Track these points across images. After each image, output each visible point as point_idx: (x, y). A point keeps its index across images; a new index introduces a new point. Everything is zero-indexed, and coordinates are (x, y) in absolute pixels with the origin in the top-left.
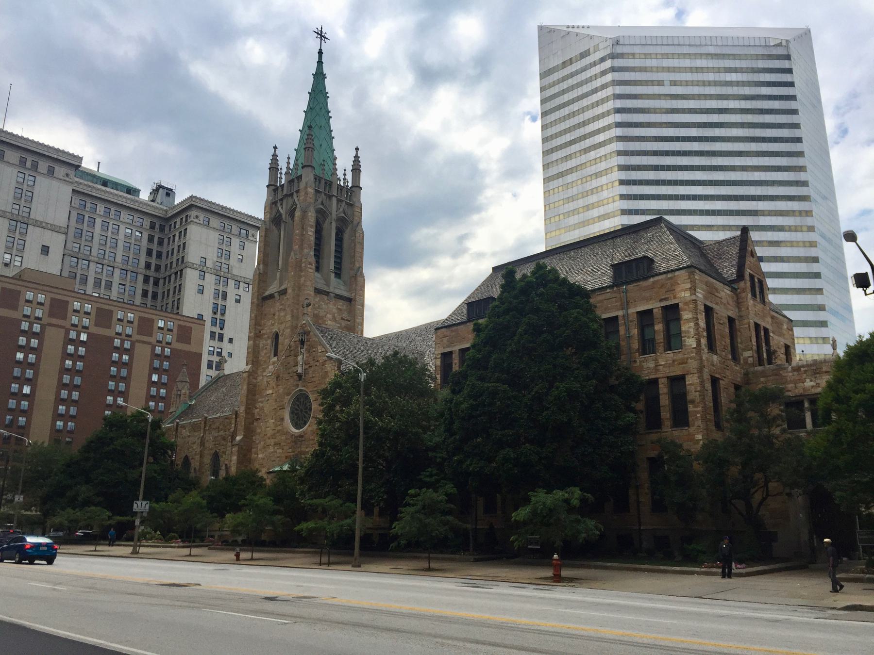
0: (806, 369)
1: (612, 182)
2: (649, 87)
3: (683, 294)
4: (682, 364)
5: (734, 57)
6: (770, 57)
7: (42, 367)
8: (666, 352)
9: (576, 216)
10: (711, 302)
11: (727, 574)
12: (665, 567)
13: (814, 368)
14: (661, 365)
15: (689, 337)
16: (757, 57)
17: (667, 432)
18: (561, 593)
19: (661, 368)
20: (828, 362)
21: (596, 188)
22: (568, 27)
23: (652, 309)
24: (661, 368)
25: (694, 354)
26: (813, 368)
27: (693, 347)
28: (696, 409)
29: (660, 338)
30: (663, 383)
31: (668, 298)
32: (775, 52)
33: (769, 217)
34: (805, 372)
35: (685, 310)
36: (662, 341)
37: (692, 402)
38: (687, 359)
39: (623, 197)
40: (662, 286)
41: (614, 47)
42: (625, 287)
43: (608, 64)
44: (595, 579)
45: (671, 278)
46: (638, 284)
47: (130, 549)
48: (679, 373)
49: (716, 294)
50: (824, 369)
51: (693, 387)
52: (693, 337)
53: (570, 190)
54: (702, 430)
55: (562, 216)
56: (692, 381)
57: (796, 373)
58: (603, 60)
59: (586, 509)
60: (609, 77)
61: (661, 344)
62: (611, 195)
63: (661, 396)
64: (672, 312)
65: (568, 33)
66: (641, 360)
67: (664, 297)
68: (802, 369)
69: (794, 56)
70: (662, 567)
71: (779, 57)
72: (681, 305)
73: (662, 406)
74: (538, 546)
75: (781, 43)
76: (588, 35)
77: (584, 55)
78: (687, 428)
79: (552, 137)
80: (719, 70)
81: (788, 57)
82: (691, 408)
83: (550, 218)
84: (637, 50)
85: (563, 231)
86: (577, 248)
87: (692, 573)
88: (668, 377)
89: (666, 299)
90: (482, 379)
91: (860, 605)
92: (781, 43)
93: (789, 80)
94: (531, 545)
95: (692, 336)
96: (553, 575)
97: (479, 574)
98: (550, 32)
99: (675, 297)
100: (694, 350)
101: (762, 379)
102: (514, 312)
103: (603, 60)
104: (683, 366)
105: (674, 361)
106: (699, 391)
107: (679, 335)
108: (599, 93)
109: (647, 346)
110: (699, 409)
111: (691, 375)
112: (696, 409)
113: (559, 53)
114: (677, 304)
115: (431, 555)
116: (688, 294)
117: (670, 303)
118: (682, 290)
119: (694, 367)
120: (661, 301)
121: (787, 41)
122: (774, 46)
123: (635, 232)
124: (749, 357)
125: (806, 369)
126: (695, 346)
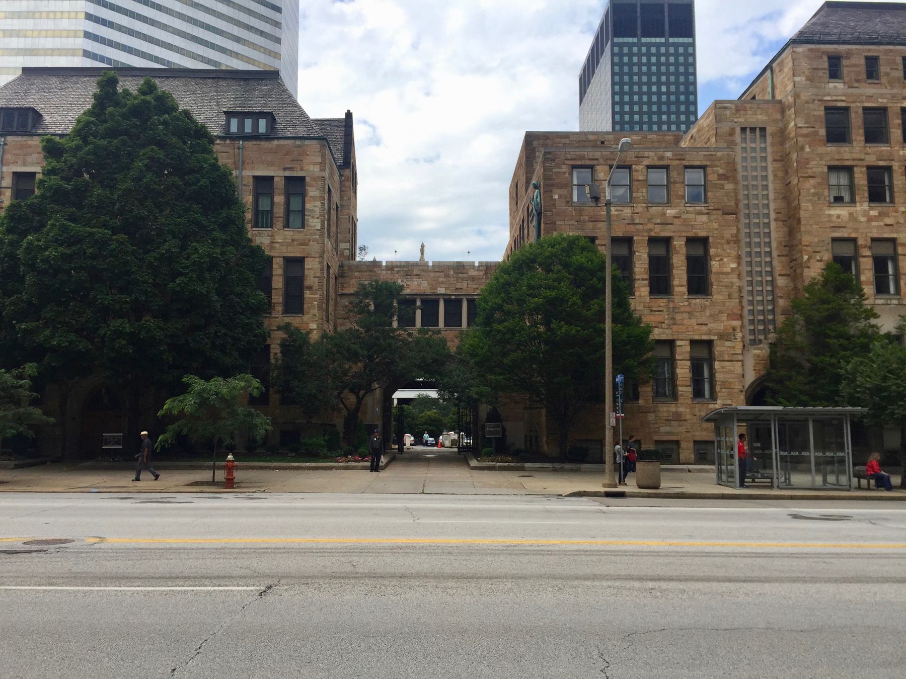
0: (399, 269)
1: (77, 12)
3: (311, 168)
4: (302, 245)
8: (285, 229)
11: (375, 468)
12: (297, 464)
13: (407, 269)
14: (278, 243)
15: (313, 217)
17: (277, 318)
18: (229, 501)
19: (277, 245)
20: (419, 266)
21: (55, 12)
23: (273, 177)
24: (277, 245)
25: (318, 237)
26: (405, 269)
27: (317, 228)
28: (312, 296)
29: (279, 211)
30: (277, 264)
31: (294, 168)
34: (398, 272)
35: (312, 186)
36: (282, 215)
37: (310, 288)
38: (309, 241)
39: (88, 35)
40: (288, 153)
42: (241, 142)
44: (27, 483)
45: (299, 146)
46: (259, 143)
48: (298, 255)
50: (416, 272)
51: (312, 272)
52: (318, 218)
54: (317, 319)
56: (312, 267)
57: (389, 272)
59: (259, 401)
61: (279, 219)
62: (73, 28)
63: (273, 278)
64: (296, 185)
66: (254, 233)
67: (288, 166)
68: (395, 269)
70: (293, 464)
72: (308, 179)
73: (275, 289)
74: (119, 444)
78: (301, 315)
82: (307, 294)
86: (163, 77)
87: (331, 468)
88: (284, 257)
89: (291, 169)
90: (72, 219)
91: (585, 492)
94: (106, 445)
95: (318, 216)
96: (225, 481)
97: (82, 485)
99: (301, 169)
100: (318, 232)
101: (356, 274)
102: (126, 137)
104: (302, 247)
105: (293, 240)
106: (317, 277)
107: (303, 212)
109: (263, 219)
110: (317, 296)
111: (312, 259)
112: (312, 296)
114: (304, 178)
115: (217, 463)
116: (317, 169)
117: (295, 175)
118: (310, 164)
119: (316, 251)
120: (285, 169)
123: (245, 79)
124: (345, 249)
125: (399, 269)
126: (319, 228)
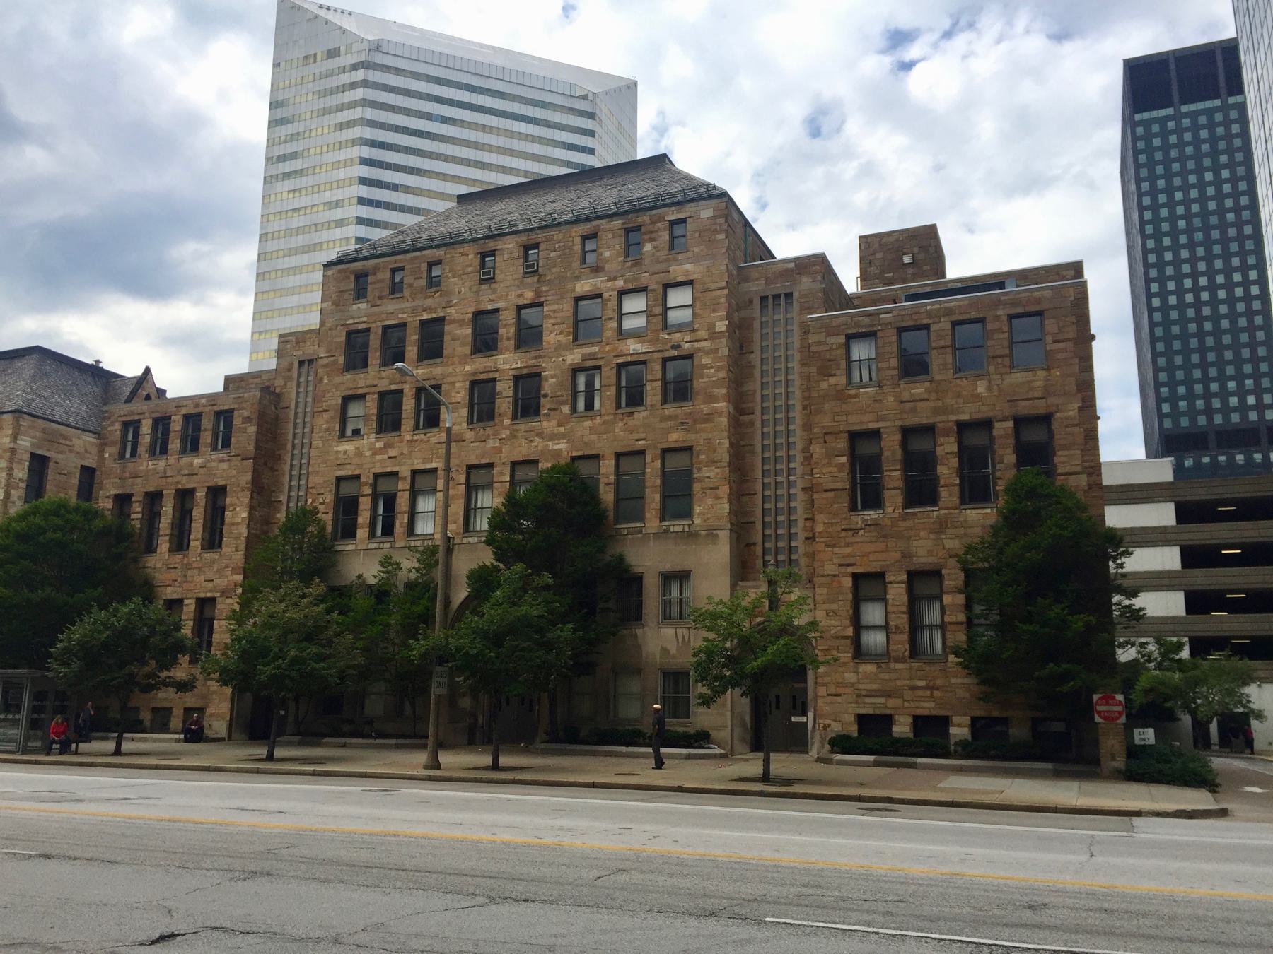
9: (298, 277)
10: (48, 450)
22: (321, 7)
41: (372, 53)
43: (360, 75)
49: (68, 443)
53: (294, 238)
55: (279, 273)
58: (355, 67)
60: (359, 93)
65: (316, 17)
71: (582, 114)
75: (587, 95)
76: (341, 28)
77: (333, 53)
79: (282, 158)
81: (591, 116)
83: (264, 273)
84: (401, 64)
85: (278, 294)
92: (587, 95)
98: (292, 8)
103: (355, 67)
108: (345, 113)
113: (302, 42)
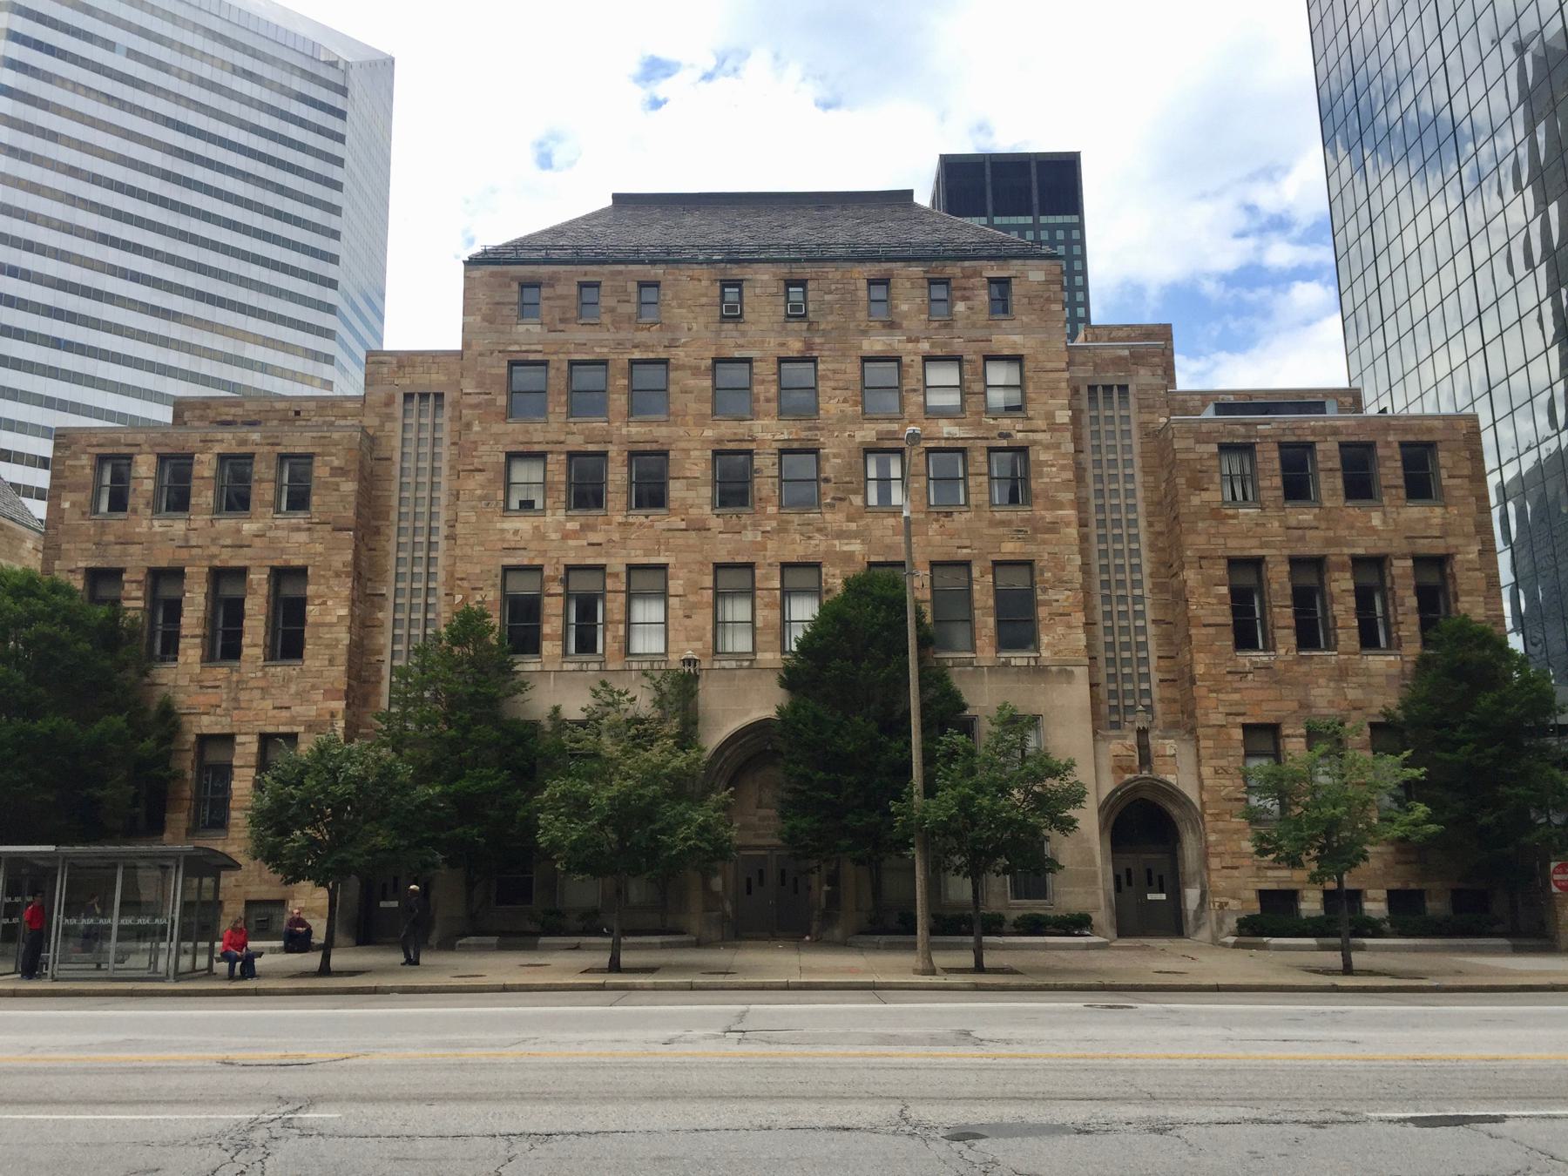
2: (185, 57)
5: (254, 54)
6: (313, 78)
7: (820, 389)
16: (293, 69)
32: (324, 72)
33: (262, 349)
47: (603, 959)
69: (355, 91)
80: (223, 65)
93: (339, 130)
121: (346, 62)
122: (324, 62)
